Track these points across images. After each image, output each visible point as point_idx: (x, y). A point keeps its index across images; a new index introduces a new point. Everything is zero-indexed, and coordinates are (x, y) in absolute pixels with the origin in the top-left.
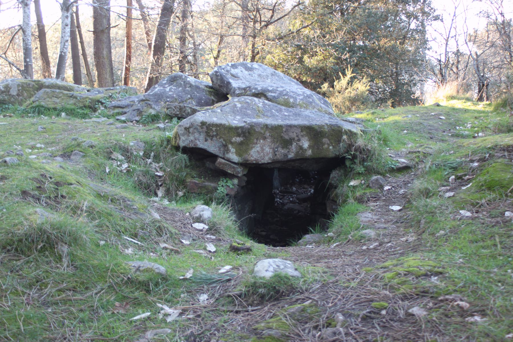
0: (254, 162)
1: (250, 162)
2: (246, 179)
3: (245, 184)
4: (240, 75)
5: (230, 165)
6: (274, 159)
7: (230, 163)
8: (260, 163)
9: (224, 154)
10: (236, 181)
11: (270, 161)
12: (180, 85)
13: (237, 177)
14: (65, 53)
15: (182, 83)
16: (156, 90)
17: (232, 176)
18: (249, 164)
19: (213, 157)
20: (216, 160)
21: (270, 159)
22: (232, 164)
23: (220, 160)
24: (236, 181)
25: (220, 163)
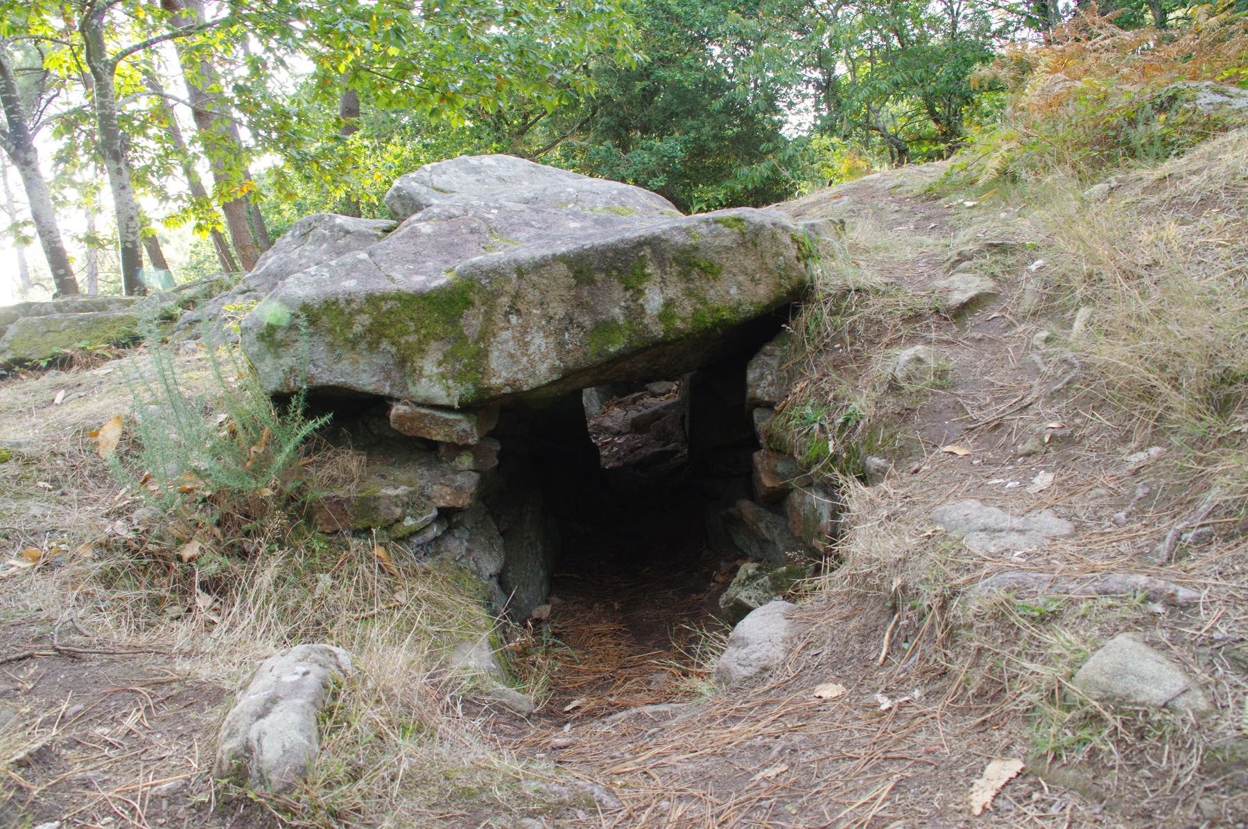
0: (508, 390)
1: (493, 393)
2: (496, 447)
3: (497, 462)
4: (456, 185)
5: (433, 417)
6: (566, 368)
7: (432, 412)
8: (525, 388)
9: (405, 387)
10: (466, 461)
11: (555, 377)
12: (323, 239)
13: (467, 447)
14: (134, 243)
15: (327, 232)
16: (270, 261)
17: (456, 449)
18: (492, 399)
19: (377, 404)
20: (389, 408)
21: (553, 369)
22: (438, 414)
23: (398, 409)
24: (466, 461)
25: (400, 417)
